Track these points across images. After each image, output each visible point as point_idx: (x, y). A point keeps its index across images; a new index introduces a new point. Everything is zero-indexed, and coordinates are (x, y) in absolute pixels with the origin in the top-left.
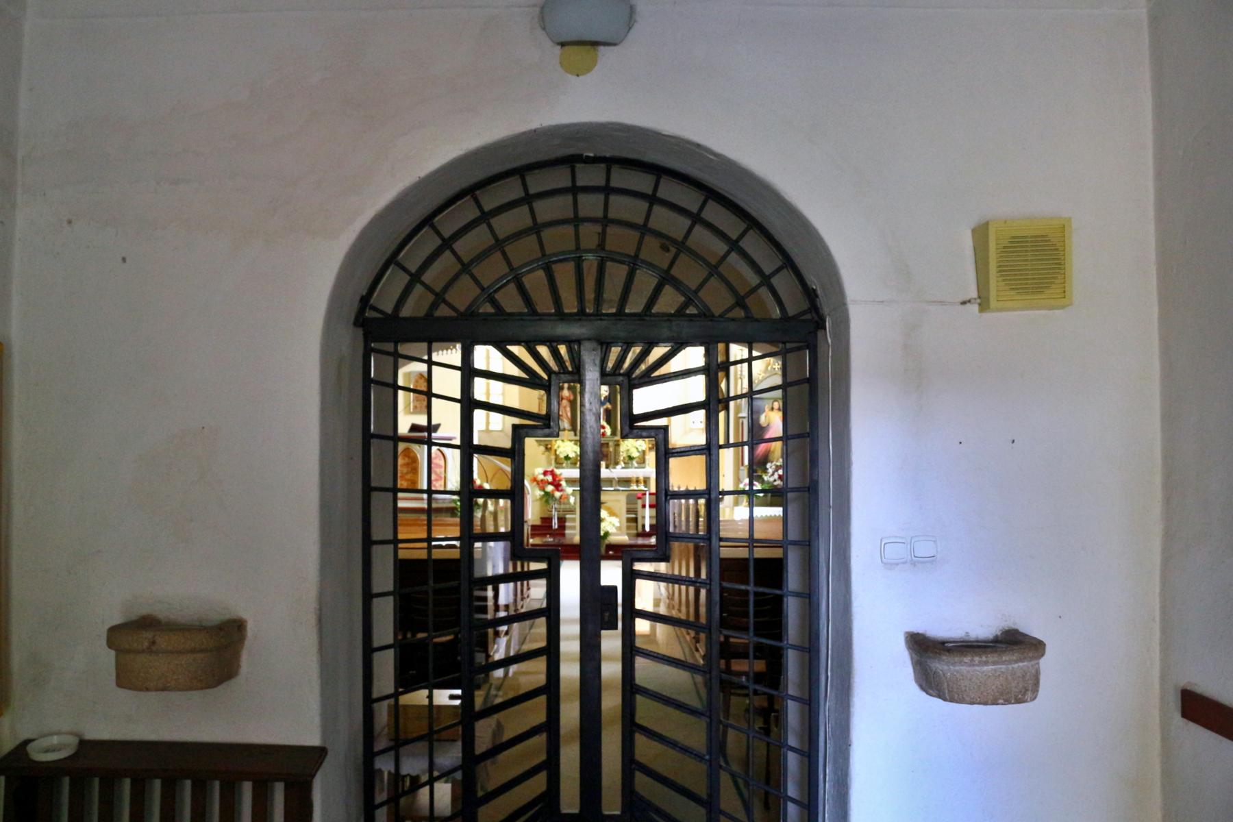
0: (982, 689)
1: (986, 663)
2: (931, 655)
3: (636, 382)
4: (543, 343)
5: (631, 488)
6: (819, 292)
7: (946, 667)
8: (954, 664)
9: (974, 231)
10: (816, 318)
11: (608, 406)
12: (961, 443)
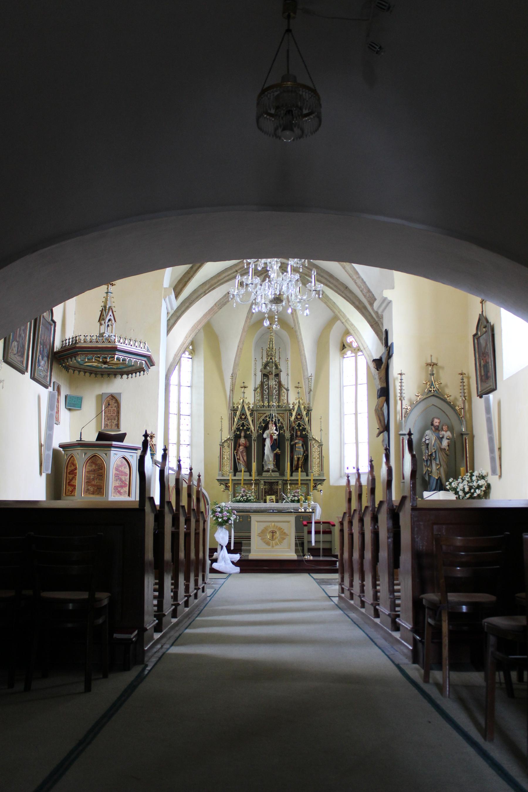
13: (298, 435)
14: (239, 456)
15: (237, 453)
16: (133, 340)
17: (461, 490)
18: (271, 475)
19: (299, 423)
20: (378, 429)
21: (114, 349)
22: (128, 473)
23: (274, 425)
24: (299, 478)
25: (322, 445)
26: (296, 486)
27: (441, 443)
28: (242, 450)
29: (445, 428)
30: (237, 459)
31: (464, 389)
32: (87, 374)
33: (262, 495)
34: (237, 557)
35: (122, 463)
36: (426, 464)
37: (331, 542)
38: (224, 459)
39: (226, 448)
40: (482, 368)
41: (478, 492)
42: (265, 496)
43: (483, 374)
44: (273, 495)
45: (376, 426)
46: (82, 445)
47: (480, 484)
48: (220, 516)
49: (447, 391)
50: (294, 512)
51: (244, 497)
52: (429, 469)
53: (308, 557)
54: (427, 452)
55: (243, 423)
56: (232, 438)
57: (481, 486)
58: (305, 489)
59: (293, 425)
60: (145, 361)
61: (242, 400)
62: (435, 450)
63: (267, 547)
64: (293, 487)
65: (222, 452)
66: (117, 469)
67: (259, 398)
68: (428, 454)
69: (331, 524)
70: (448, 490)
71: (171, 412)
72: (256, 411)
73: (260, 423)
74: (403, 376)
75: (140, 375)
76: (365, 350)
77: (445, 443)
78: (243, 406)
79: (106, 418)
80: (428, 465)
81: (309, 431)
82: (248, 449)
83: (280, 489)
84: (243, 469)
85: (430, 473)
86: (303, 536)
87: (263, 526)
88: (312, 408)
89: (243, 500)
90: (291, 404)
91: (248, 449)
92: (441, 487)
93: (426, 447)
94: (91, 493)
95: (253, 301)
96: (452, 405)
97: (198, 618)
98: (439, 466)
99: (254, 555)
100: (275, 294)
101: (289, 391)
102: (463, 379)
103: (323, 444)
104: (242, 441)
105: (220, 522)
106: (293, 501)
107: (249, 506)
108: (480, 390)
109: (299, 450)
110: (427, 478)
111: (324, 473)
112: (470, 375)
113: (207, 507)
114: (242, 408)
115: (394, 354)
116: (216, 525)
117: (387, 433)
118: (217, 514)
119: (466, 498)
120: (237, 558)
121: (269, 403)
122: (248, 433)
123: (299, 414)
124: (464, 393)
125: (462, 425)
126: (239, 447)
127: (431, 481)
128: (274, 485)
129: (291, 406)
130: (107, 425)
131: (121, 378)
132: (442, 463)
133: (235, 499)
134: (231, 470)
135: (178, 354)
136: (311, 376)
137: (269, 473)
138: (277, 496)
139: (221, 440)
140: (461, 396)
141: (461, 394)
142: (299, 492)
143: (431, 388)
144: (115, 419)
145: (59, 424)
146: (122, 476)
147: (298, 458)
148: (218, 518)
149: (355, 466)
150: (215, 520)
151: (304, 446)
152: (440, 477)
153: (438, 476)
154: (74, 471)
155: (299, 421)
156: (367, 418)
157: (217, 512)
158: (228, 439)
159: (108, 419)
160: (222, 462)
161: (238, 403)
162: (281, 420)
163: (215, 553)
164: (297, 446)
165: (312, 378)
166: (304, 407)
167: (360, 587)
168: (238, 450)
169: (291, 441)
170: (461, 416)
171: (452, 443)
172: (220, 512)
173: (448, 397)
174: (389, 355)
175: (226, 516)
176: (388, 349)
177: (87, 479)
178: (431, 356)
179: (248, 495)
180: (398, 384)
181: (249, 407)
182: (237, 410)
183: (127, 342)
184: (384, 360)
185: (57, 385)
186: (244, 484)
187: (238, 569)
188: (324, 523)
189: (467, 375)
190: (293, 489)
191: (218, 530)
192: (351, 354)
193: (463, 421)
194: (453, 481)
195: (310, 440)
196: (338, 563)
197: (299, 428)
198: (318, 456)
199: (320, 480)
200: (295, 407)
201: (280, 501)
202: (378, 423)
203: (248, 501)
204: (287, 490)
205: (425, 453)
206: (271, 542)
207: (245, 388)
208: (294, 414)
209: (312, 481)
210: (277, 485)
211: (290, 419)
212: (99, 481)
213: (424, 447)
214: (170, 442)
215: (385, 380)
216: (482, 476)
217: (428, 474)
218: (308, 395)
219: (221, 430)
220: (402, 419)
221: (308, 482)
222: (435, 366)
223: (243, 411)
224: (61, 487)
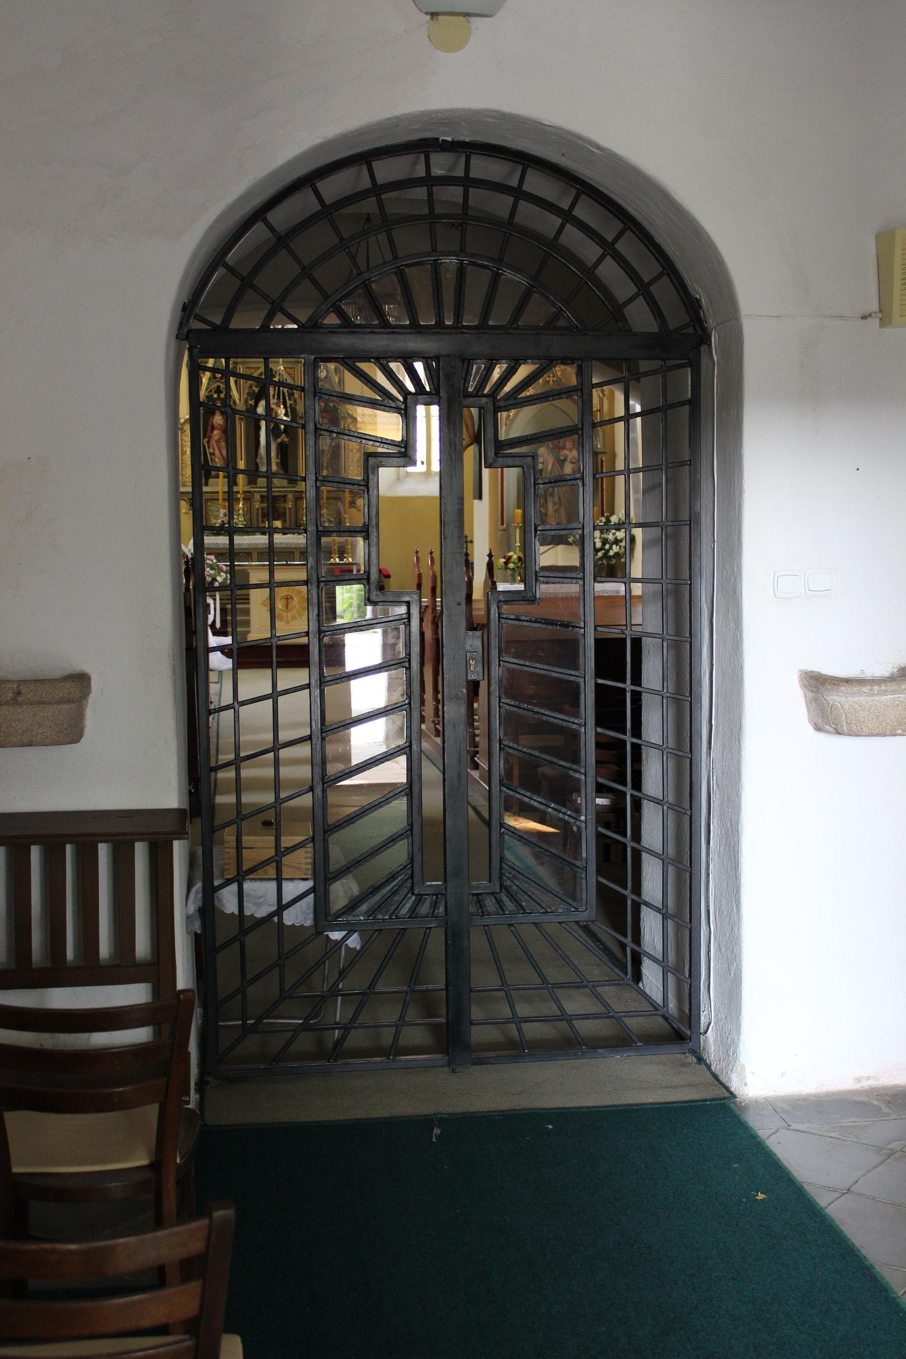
0: (881, 719)
1: (885, 693)
2: (829, 687)
3: (502, 404)
4: (395, 359)
6: (703, 302)
7: (844, 699)
8: (853, 695)
9: (878, 237)
10: (700, 332)
11: (284, 438)
12: (858, 469)
14: (214, 449)
15: (208, 442)
23: (282, 406)
28: (218, 437)
30: (210, 453)
38: (186, 453)
41: (615, 549)
52: (542, 510)
55: (219, 387)
57: (621, 541)
70: (568, 544)
83: (290, 508)
98: (558, 506)
117: (478, 447)
128: (280, 501)
143: (549, 377)
167: (434, 710)
168: (210, 438)
206: (285, 614)
210: (285, 501)
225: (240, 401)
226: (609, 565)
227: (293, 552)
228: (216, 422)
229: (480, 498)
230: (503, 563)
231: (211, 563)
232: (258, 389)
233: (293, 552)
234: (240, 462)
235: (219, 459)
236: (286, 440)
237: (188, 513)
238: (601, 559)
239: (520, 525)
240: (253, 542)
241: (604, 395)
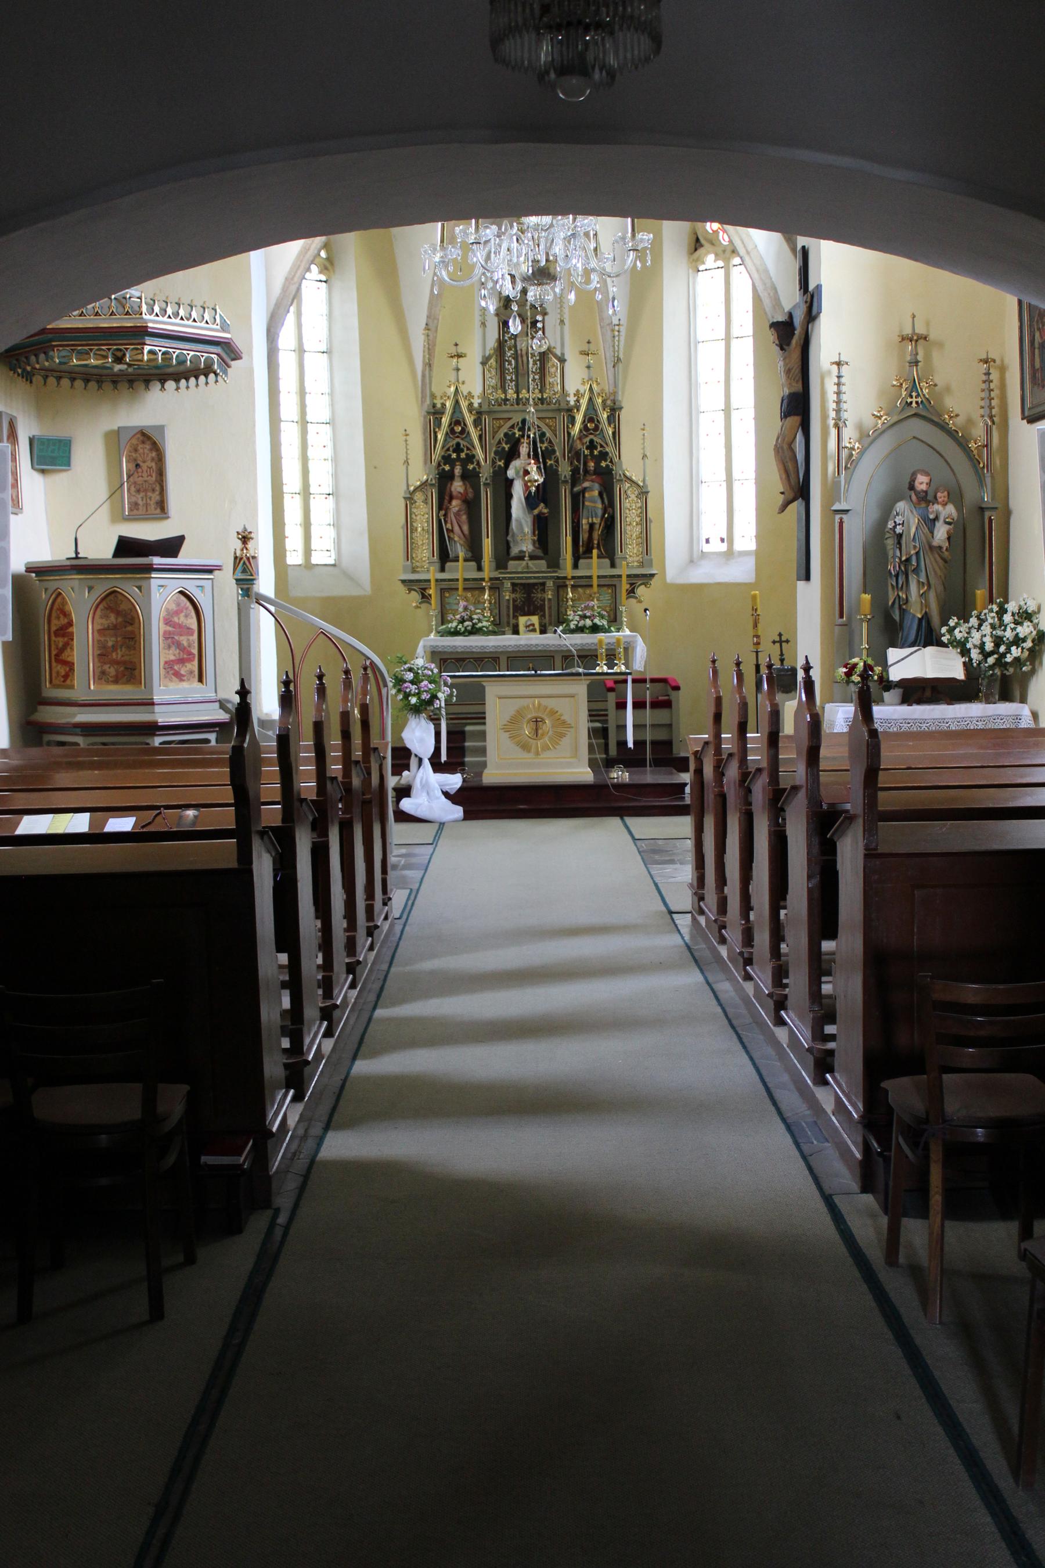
5: (598, 670)
13: (588, 469)
14: (452, 524)
15: (445, 515)
16: (186, 305)
17: (975, 646)
18: (528, 566)
19: (592, 441)
20: (782, 493)
21: (141, 333)
22: (195, 626)
24: (595, 572)
25: (647, 492)
26: (588, 591)
27: (932, 533)
28: (457, 509)
29: (942, 496)
30: (447, 530)
31: (991, 390)
32: (79, 384)
33: (508, 615)
34: (454, 781)
35: (178, 605)
36: (894, 584)
37: (670, 726)
38: (416, 530)
39: (420, 505)
40: (1037, 351)
42: (516, 617)
43: (1037, 365)
44: (533, 614)
45: (777, 483)
46: (80, 567)
47: (1021, 636)
48: (412, 692)
49: (951, 403)
50: (585, 674)
51: (467, 623)
52: (900, 594)
53: (618, 774)
54: (898, 554)
55: (458, 444)
56: (434, 482)
57: (1024, 640)
58: (608, 597)
59: (578, 445)
60: (218, 355)
61: (453, 389)
62: (917, 550)
63: (526, 755)
64: (579, 593)
65: (411, 514)
66: (168, 622)
67: (494, 381)
68: (900, 559)
69: (670, 685)
70: (941, 644)
71: (283, 417)
72: (489, 413)
73: (499, 442)
74: (844, 369)
75: (207, 383)
76: (750, 257)
77: (941, 533)
78: (457, 402)
79: (133, 489)
80: (900, 586)
81: (616, 460)
82: (472, 505)
83: (550, 600)
84: (461, 555)
85: (905, 604)
86: (606, 710)
87: (512, 707)
88: (623, 405)
89: (463, 629)
90: (572, 395)
91: (472, 505)
92: (928, 637)
93: (896, 541)
94: (111, 679)
95: (481, 278)
96: (960, 439)
97: (379, 1013)
99: (492, 776)
100: (535, 261)
101: (566, 363)
102: (988, 374)
103: (649, 489)
104: (457, 486)
105: (415, 705)
106: (580, 630)
107: (479, 644)
108: (1028, 405)
109: (592, 505)
110: (897, 617)
111: (651, 560)
112: (1006, 361)
113: (384, 691)
114: (454, 408)
115: (821, 314)
116: (406, 712)
118: (407, 688)
119: (987, 665)
120: (456, 783)
121: (517, 392)
122: (471, 467)
123: (591, 420)
124: (991, 408)
125: (982, 487)
126: (450, 502)
127: (907, 623)
128: (536, 590)
129: (572, 400)
130: (136, 504)
131: (161, 390)
132: (932, 581)
133: (444, 627)
134: (433, 556)
135: (294, 276)
136: (618, 325)
137: (524, 563)
138: (544, 616)
139: (408, 486)
140: (983, 416)
141: (982, 411)
142: (593, 606)
143: (912, 397)
144: (153, 490)
145: (22, 513)
146: (181, 635)
147: (592, 526)
148: (407, 696)
149: (725, 536)
150: (401, 700)
151: (605, 496)
152: (926, 613)
153: (924, 612)
154: (67, 628)
155: (591, 437)
156: (754, 485)
157: (405, 681)
158: (424, 484)
159: (138, 491)
160: (412, 538)
161: (445, 395)
162: (548, 435)
163: (405, 773)
164: (587, 495)
165: (622, 329)
166: (604, 402)
168: (447, 510)
169: (573, 485)
170: (981, 465)
171: (959, 532)
172: (412, 682)
173: (951, 417)
174: (812, 315)
175: (426, 691)
176: (809, 300)
177: (100, 648)
178: (914, 316)
179: (475, 616)
180: (831, 388)
181: (471, 405)
182: (443, 413)
183: (169, 311)
184: (798, 320)
185: (9, 419)
186: (465, 589)
187: (458, 811)
188: (653, 681)
189: (998, 362)
190: (579, 599)
191: (409, 722)
192: (715, 261)
193: (984, 476)
194: (957, 625)
195: (619, 480)
196: (688, 789)
197: (592, 453)
198: (638, 519)
199: (644, 576)
200: (581, 401)
201: (551, 628)
202: (781, 478)
203: (474, 631)
204: (567, 601)
205: (894, 557)
207: (461, 356)
208: (579, 418)
209: (624, 579)
210: (543, 590)
211: (570, 431)
212: (127, 652)
213: (890, 543)
214: (285, 491)
215: (800, 375)
216: (1026, 612)
217: (900, 607)
218: (612, 369)
219: (407, 462)
220: (838, 474)
221: (614, 581)
222: (921, 341)
223: (457, 414)
224: (39, 667)
225: (486, 462)
226: (1003, 675)
227: (553, 657)
228: (456, 489)
229: (807, 578)
230: (843, 675)
231: (430, 673)
232: (508, 446)
233: (553, 657)
234: (486, 540)
235: (459, 537)
236: (545, 511)
237: (420, 607)
238: (992, 667)
239: (869, 617)
240: (501, 644)
241: (993, 423)
